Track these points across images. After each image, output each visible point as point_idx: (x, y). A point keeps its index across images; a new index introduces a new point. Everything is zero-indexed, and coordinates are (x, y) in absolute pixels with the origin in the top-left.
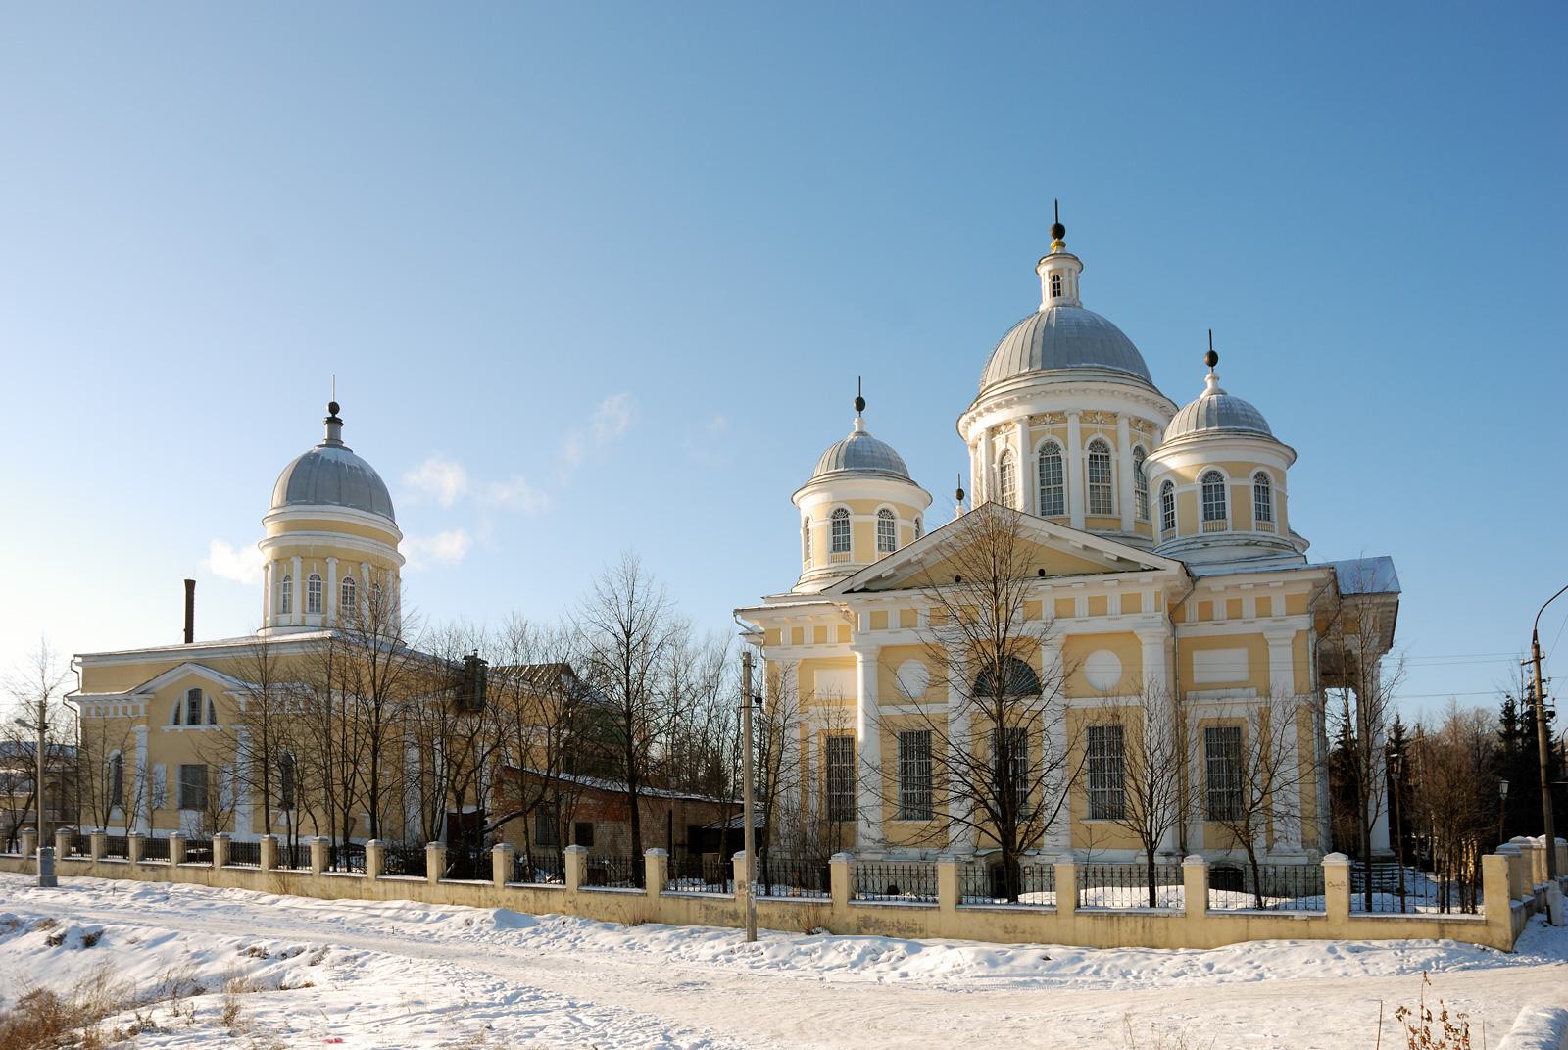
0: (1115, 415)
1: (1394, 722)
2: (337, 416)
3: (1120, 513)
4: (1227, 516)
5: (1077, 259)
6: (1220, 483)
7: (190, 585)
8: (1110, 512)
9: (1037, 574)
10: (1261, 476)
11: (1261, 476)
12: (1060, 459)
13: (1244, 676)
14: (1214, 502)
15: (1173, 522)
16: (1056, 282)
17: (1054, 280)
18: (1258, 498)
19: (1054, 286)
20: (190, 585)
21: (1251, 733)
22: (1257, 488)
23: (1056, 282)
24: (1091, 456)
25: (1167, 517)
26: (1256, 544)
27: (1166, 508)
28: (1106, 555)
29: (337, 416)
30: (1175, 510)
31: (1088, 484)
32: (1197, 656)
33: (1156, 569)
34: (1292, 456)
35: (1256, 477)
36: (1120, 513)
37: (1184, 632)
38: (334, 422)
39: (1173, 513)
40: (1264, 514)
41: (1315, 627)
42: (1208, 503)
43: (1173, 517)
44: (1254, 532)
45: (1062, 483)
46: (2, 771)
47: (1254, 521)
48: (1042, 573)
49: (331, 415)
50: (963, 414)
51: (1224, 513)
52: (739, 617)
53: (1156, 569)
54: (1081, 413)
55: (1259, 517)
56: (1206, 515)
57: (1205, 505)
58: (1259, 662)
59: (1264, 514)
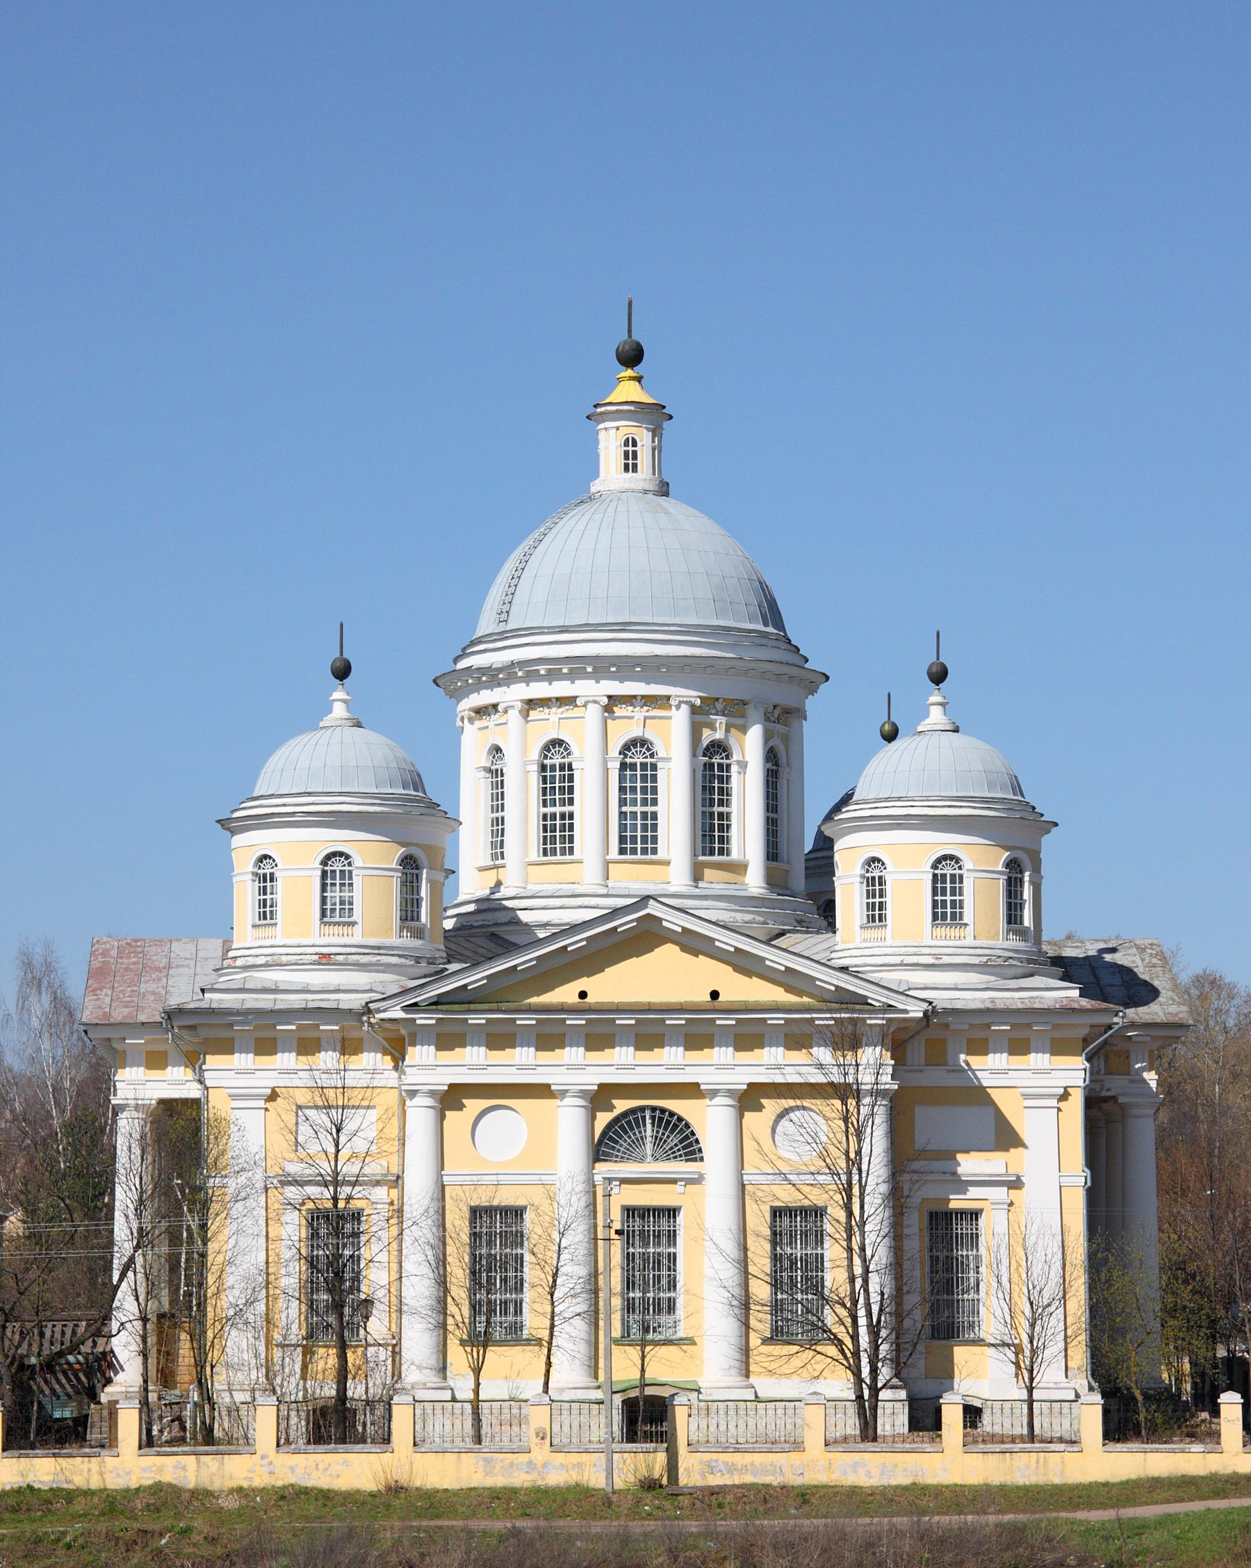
17: (626, 443)
19: (626, 454)
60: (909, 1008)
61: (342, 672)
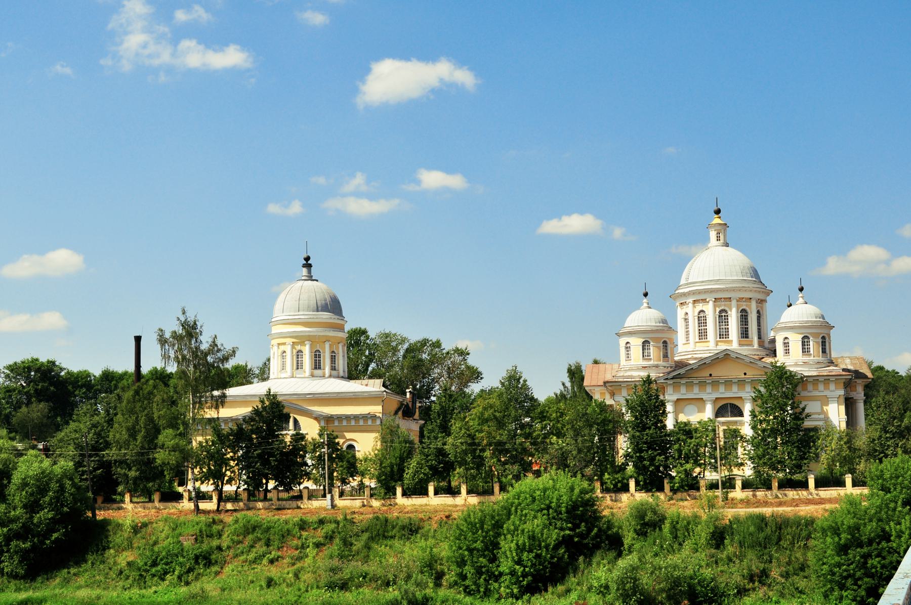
2: (309, 262)
7: (138, 339)
20: (138, 339)
29: (309, 262)
38: (308, 266)
49: (305, 262)
61: (646, 295)
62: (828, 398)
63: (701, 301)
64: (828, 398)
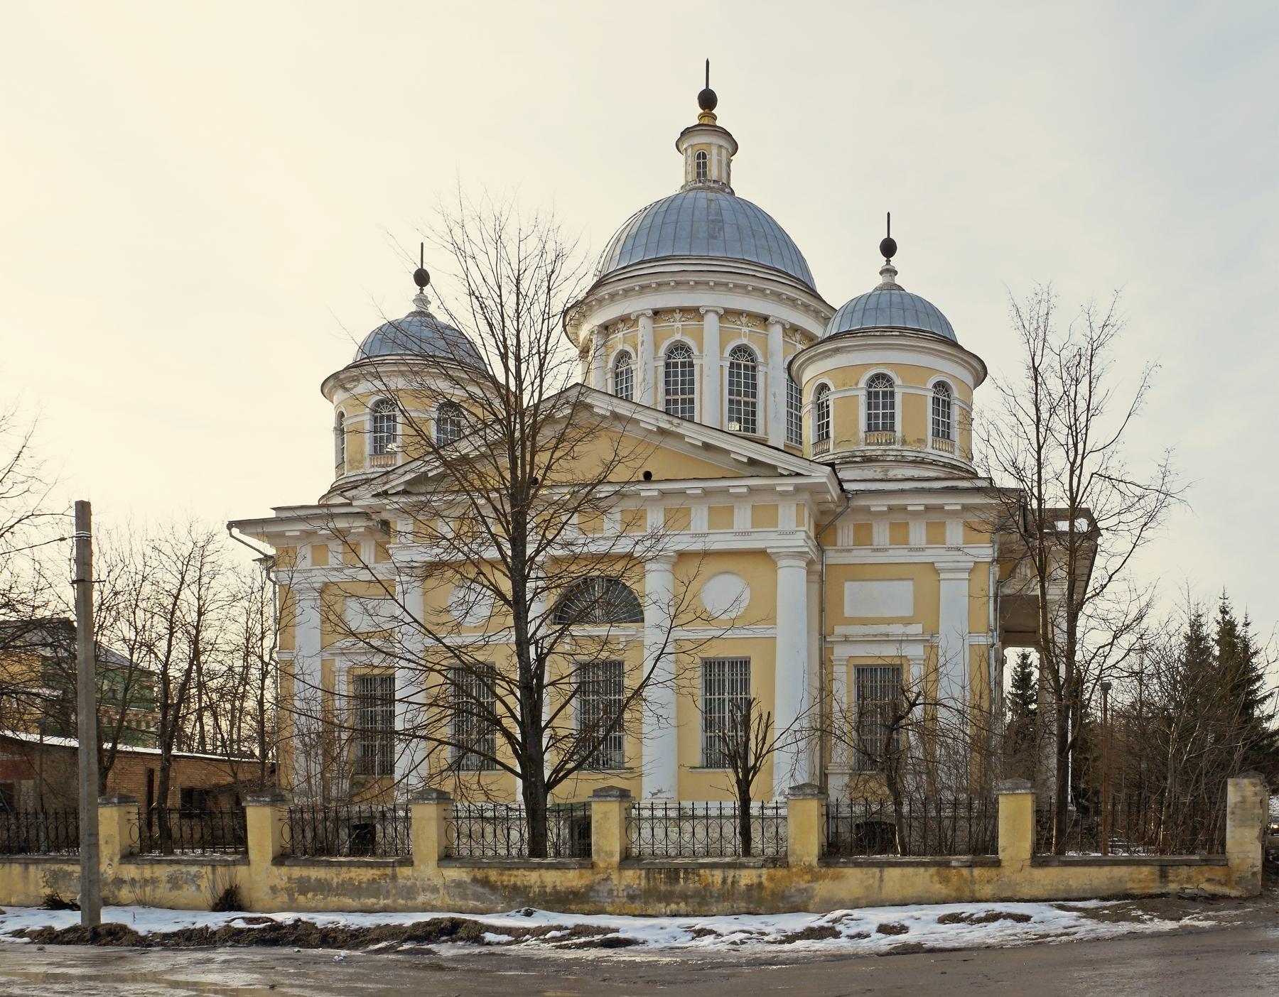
0: (766, 319)
1: (1187, 629)
3: (766, 433)
4: (896, 428)
5: (729, 135)
6: (751, 400)
8: (754, 431)
9: (642, 478)
10: (941, 386)
11: (941, 386)
12: (691, 365)
13: (907, 611)
14: (881, 411)
15: (827, 432)
16: (701, 161)
17: (699, 157)
18: (937, 412)
19: (698, 164)
21: (914, 673)
22: (936, 401)
23: (701, 161)
24: (732, 364)
25: (820, 427)
26: (931, 464)
27: (821, 417)
28: (732, 456)
30: (831, 419)
31: (726, 397)
32: (849, 588)
33: (798, 474)
34: (980, 372)
35: (935, 386)
36: (766, 433)
37: (833, 557)
39: (828, 422)
40: (942, 432)
41: (999, 560)
42: (873, 412)
43: (828, 427)
44: (930, 450)
45: (693, 393)
46: (5, 758)
47: (930, 439)
48: (648, 476)
50: (882, 955)
51: (892, 425)
52: (235, 531)
53: (798, 474)
54: (722, 312)
55: (936, 434)
56: (869, 425)
57: (869, 415)
58: (928, 608)
59: (942, 432)
60: (813, 474)
62: (937, 572)
63: (621, 326)
64: (937, 572)
